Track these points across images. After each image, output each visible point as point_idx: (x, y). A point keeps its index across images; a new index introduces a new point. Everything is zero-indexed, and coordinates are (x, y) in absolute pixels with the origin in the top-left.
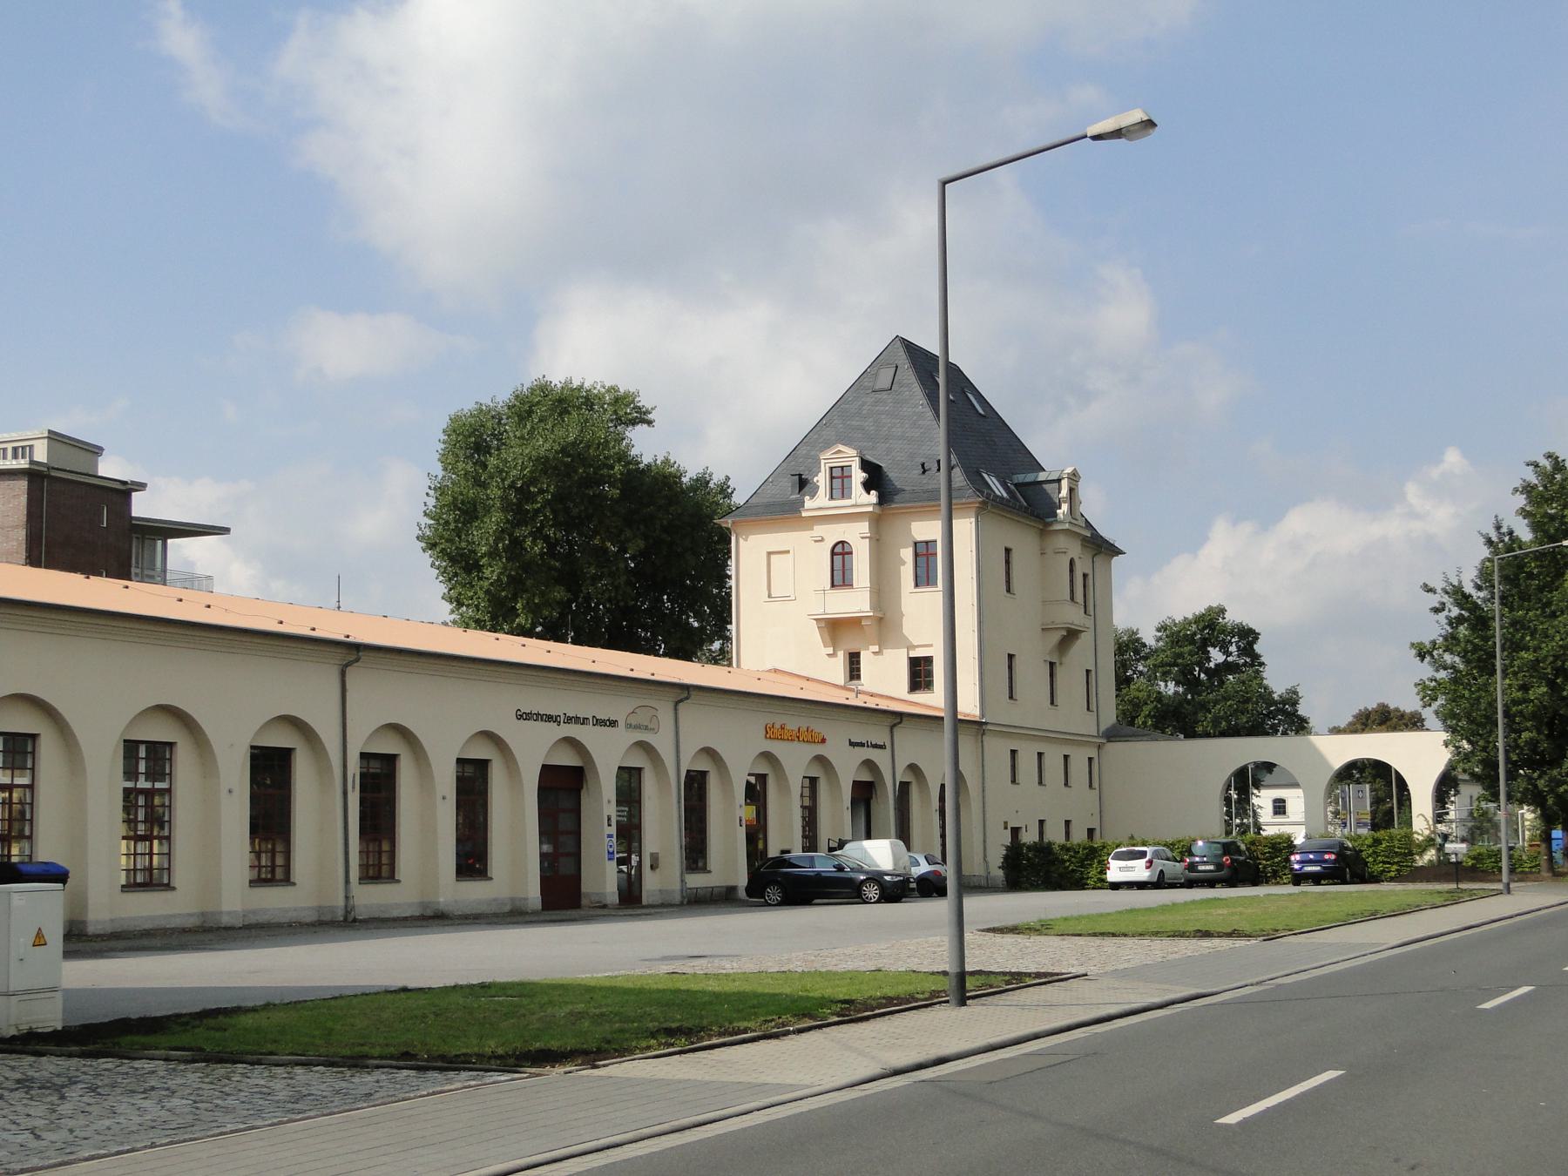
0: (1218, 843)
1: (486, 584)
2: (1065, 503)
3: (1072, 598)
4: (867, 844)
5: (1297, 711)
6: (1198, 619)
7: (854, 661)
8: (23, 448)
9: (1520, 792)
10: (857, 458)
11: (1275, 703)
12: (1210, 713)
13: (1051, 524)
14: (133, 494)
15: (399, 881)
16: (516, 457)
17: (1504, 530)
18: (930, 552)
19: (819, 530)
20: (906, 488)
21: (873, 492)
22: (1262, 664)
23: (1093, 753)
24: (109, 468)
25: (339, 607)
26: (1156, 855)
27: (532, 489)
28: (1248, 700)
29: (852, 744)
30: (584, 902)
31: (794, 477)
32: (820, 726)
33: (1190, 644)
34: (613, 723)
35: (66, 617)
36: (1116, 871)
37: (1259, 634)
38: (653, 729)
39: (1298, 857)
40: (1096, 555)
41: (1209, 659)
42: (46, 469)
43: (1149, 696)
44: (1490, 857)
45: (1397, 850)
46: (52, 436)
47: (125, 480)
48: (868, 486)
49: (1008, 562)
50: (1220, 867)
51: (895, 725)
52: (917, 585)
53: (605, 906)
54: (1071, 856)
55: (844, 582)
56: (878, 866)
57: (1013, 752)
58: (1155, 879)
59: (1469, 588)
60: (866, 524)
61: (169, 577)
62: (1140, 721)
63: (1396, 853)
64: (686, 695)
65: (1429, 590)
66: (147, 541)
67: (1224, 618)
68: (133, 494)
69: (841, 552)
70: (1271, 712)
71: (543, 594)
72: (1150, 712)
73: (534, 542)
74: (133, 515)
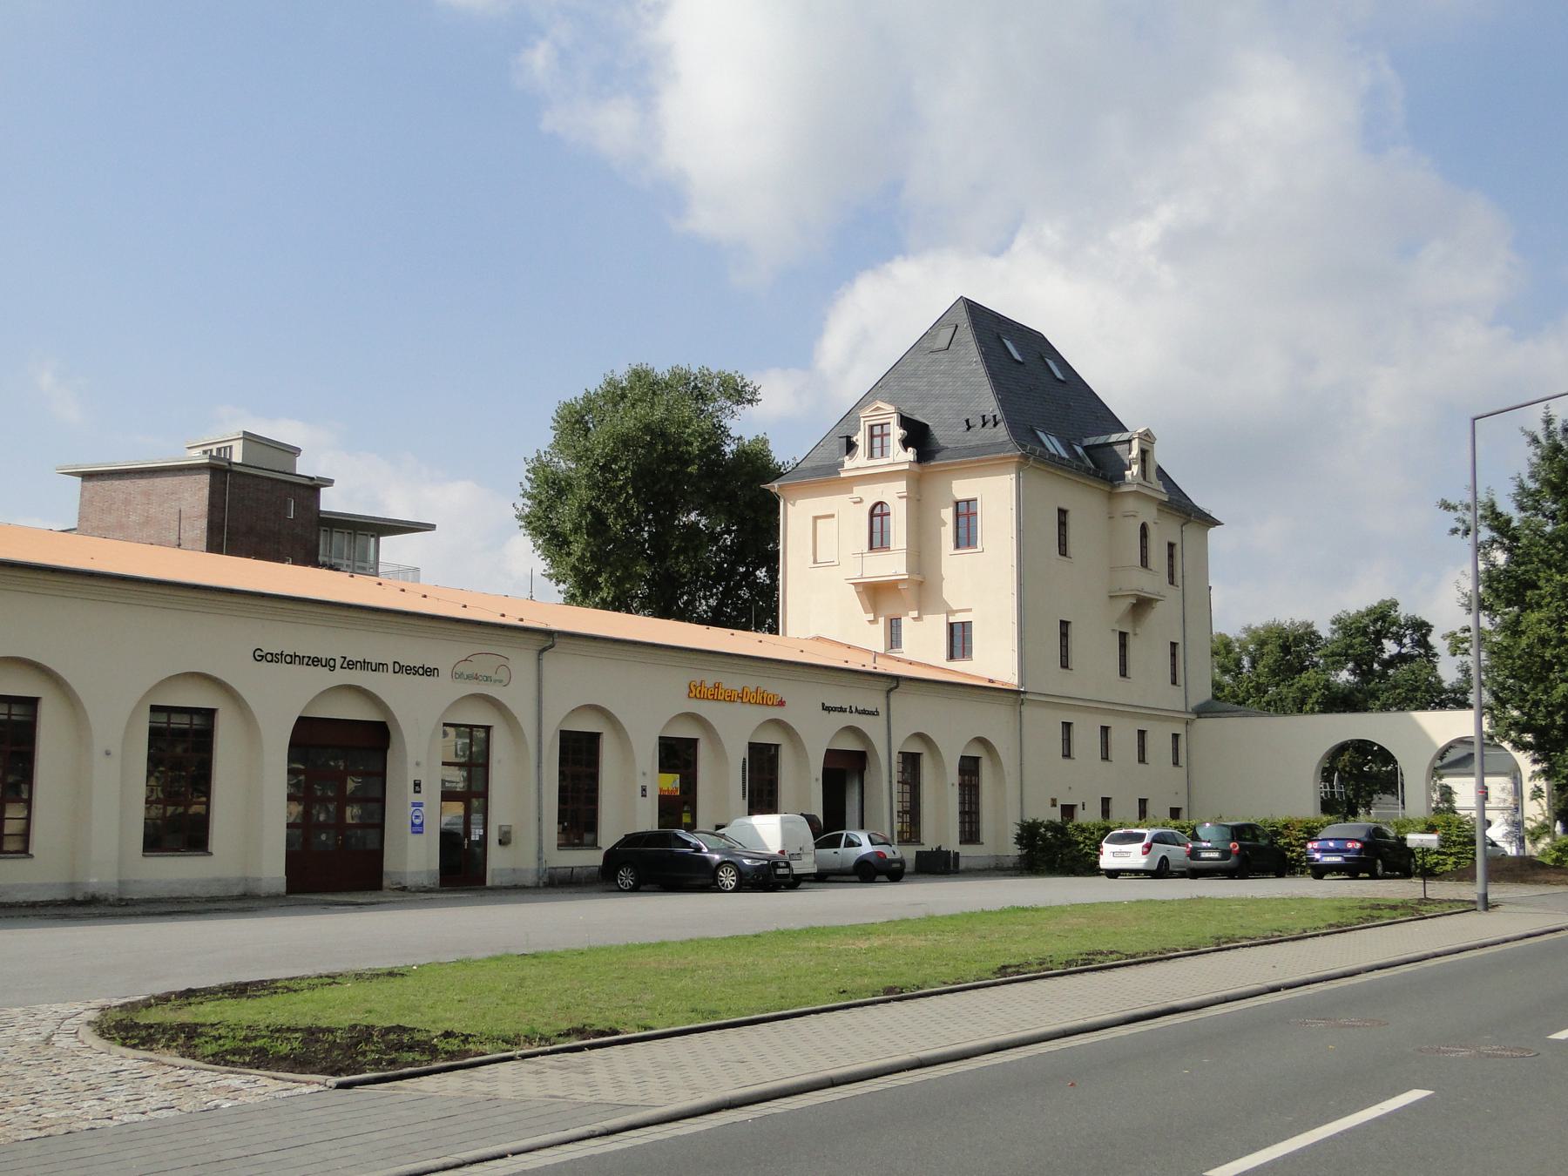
1: (573, 559)
3: (1144, 562)
4: (757, 820)
5: (1468, 700)
6: (1370, 612)
8: (225, 448)
10: (895, 415)
11: (1445, 691)
12: (1379, 700)
14: (322, 489)
15: (32, 856)
16: (600, 439)
18: (971, 511)
19: (859, 491)
20: (949, 446)
21: (910, 449)
22: (1435, 655)
23: (1179, 729)
24: (305, 467)
25: (531, 597)
26: (1158, 839)
27: (613, 466)
28: (1417, 689)
29: (826, 708)
30: (386, 883)
31: (841, 439)
32: (775, 686)
33: (1362, 635)
34: (429, 672)
35: (335, 612)
36: (1110, 856)
37: (1432, 626)
38: (501, 681)
39: (1316, 845)
40: (1184, 524)
41: (1382, 650)
42: (226, 464)
43: (1318, 684)
45: (1454, 838)
47: (312, 476)
48: (906, 443)
50: (1226, 854)
51: (891, 690)
52: (957, 546)
53: (404, 889)
54: (1086, 838)
55: (882, 544)
56: (769, 850)
58: (1154, 867)
59: (1507, 507)
60: (904, 483)
63: (1454, 842)
65: (1447, 506)
66: (358, 536)
68: (322, 489)
69: (878, 513)
70: (1442, 700)
71: (626, 568)
74: (321, 509)
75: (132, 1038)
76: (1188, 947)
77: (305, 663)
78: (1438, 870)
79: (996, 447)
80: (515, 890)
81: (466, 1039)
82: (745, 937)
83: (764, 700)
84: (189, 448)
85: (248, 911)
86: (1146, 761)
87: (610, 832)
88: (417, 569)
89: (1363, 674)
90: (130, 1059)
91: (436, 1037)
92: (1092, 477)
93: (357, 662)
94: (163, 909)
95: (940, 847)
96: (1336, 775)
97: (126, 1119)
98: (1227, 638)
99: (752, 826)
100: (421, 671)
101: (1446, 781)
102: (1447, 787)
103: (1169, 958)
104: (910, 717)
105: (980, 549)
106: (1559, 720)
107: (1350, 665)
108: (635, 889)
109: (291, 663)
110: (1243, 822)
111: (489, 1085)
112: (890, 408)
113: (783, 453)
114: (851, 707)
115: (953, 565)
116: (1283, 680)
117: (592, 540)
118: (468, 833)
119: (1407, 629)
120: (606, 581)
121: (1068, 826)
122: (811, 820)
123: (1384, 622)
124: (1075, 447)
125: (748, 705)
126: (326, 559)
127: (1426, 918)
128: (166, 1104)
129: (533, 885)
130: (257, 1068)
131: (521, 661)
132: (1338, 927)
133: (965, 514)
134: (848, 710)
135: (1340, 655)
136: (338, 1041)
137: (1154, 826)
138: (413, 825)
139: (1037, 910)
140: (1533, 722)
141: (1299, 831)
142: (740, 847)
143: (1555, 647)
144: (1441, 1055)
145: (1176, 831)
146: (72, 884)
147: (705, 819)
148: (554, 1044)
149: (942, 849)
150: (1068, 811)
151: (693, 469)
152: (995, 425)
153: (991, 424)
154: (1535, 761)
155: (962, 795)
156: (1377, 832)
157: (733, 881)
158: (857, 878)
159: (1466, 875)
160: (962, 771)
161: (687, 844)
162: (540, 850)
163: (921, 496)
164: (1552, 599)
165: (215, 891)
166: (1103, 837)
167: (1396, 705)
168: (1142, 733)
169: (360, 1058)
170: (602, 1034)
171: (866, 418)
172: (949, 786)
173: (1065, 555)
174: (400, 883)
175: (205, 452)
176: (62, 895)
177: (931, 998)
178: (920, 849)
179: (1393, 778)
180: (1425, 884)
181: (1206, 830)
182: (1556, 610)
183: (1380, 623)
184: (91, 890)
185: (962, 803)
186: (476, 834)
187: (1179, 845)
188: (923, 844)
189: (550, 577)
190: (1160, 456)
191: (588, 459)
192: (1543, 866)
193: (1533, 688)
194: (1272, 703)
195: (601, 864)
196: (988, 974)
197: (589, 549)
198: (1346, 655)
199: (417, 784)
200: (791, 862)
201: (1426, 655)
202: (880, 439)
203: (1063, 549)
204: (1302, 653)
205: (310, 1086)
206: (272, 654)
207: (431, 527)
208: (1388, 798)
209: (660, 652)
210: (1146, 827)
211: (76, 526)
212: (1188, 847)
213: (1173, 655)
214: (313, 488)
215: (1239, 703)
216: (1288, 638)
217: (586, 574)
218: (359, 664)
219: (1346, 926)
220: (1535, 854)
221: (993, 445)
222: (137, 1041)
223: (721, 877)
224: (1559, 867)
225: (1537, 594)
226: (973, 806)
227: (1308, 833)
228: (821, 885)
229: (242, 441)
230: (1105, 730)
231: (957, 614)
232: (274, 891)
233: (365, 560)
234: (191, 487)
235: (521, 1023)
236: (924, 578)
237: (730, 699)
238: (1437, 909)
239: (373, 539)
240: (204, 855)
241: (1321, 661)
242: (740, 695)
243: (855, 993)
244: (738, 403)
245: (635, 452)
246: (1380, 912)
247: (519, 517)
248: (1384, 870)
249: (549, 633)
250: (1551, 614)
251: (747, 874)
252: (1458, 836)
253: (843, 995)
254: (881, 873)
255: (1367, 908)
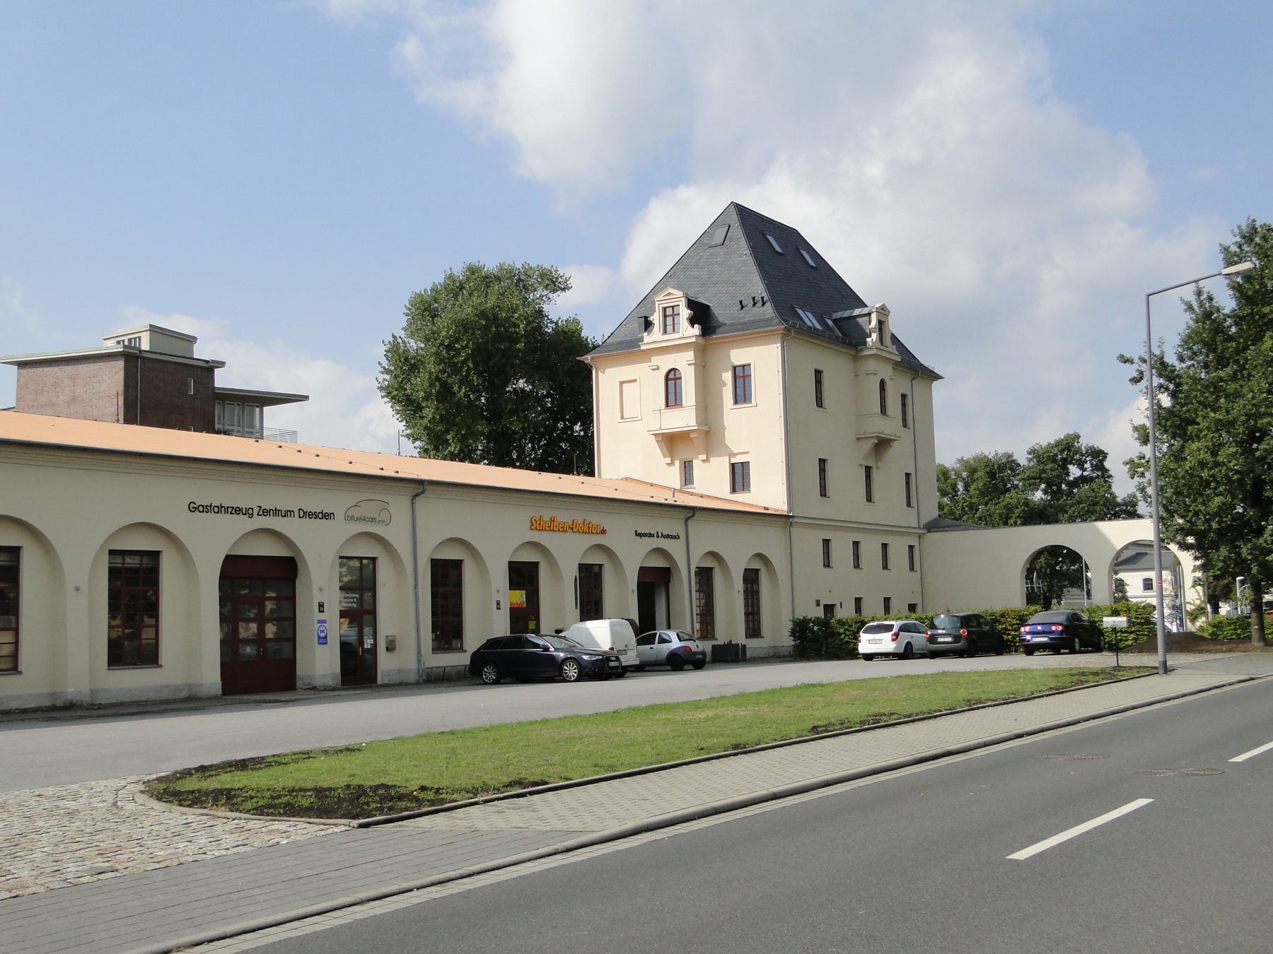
0: (956, 616)
1: (426, 421)
2: (874, 332)
4: (592, 625)
5: (1136, 511)
6: (1058, 443)
7: (687, 468)
8: (135, 339)
9: (1221, 561)
10: (684, 298)
11: (1119, 505)
12: (1067, 513)
13: (862, 350)
14: (216, 370)
15: (763, 637)
16: (444, 324)
17: (1204, 296)
19: (656, 360)
21: (696, 326)
22: (1110, 476)
24: (202, 352)
25: (399, 453)
27: (456, 345)
28: (1096, 503)
29: (638, 535)
30: (299, 684)
32: (598, 518)
33: (1053, 462)
34: (327, 516)
36: (867, 643)
37: (1107, 454)
38: (383, 521)
39: (1027, 629)
41: (1068, 474)
42: (138, 352)
43: (1019, 502)
44: (1230, 624)
46: (154, 329)
47: (208, 359)
48: (692, 321)
49: (904, 405)
50: (957, 639)
52: (736, 402)
53: (314, 688)
54: (846, 630)
56: (600, 647)
57: (856, 544)
59: (1171, 359)
60: (692, 353)
61: (265, 433)
62: (1012, 521)
64: (421, 490)
67: (1079, 442)
68: (216, 370)
69: (672, 377)
70: (1116, 512)
71: (469, 428)
72: (1019, 514)
73: (460, 388)
74: (216, 385)
75: (185, 800)
76: (948, 708)
77: (229, 512)
78: (1122, 645)
79: (766, 322)
80: (400, 686)
81: (438, 790)
82: (607, 714)
83: (589, 530)
84: (105, 339)
85: (198, 709)
86: (889, 568)
87: (474, 638)
88: (294, 432)
89: (1053, 493)
90: (177, 816)
91: (415, 791)
92: (840, 344)
93: (270, 510)
94: (129, 710)
95: (731, 641)
96: (1035, 573)
97: (217, 853)
98: (945, 467)
99: (587, 629)
100: (320, 516)
101: (1121, 575)
102: (1121, 580)
103: (935, 717)
104: (705, 539)
105: (754, 403)
106: (1215, 526)
107: (1043, 486)
108: (497, 682)
109: (218, 512)
110: (969, 613)
111: (468, 822)
112: (679, 293)
113: (593, 332)
114: (657, 533)
115: (733, 418)
116: (991, 500)
117: (440, 405)
118: (361, 643)
119: (1088, 457)
120: (454, 438)
121: (832, 621)
122: (631, 622)
123: (1069, 451)
124: (827, 320)
125: (577, 534)
126: (221, 426)
127: (1121, 681)
128: (241, 843)
129: (415, 682)
130: (294, 816)
131: (399, 505)
132: (1057, 689)
133: (742, 376)
134: (655, 535)
135: (1035, 478)
136: (342, 796)
137: (899, 619)
138: (319, 638)
139: (823, 686)
140: (1195, 527)
141: (1013, 618)
142: (579, 646)
143: (1211, 469)
144: (1154, 775)
145: (917, 622)
146: (54, 694)
147: (545, 626)
148: (504, 792)
149: (733, 643)
150: (829, 609)
151: (520, 346)
152: (763, 304)
153: (760, 304)
154: (1196, 558)
155: (746, 599)
156: (1074, 618)
157: (575, 673)
158: (669, 668)
159: (1150, 647)
160: (746, 581)
161: (537, 646)
162: (419, 653)
163: (706, 363)
164: (1208, 431)
165: (165, 695)
166: (859, 629)
167: (1080, 517)
168: (885, 546)
169: (366, 807)
170: (536, 784)
171: (660, 302)
172: (630, 593)
173: (821, 407)
174: (310, 684)
175: (118, 342)
176: (46, 703)
177: (767, 751)
178: (715, 643)
179: (1079, 575)
180: (1117, 655)
181: (941, 620)
182: (1212, 440)
183: (1066, 452)
184: (69, 698)
185: (746, 605)
186: (368, 643)
187: (920, 633)
188: (717, 639)
189: (408, 436)
190: (893, 326)
191: (435, 340)
192: (1203, 639)
193: (1195, 500)
194: (983, 518)
195: (469, 663)
196: (805, 733)
197: (439, 412)
198: (1040, 478)
199: (321, 606)
200: (620, 656)
201: (1103, 476)
202: (671, 318)
203: (819, 402)
204: (1005, 478)
205: (338, 827)
206: (203, 506)
207: (305, 398)
208: (1075, 591)
209: (334, 478)
210: (893, 620)
211: (15, 405)
212: (927, 634)
213: (908, 483)
214: (208, 369)
215: (956, 519)
216: (994, 466)
217: (436, 434)
218: (271, 511)
219: (1063, 689)
220: (1195, 631)
221: (760, 321)
222: (190, 802)
223: (565, 670)
224: (1215, 639)
225: (1196, 429)
226: (755, 608)
227: (1020, 620)
228: (639, 674)
229: (149, 332)
230: (856, 544)
231: (737, 456)
232: (213, 694)
233: (252, 426)
234: (109, 371)
235: (472, 779)
236: (710, 428)
237: (563, 529)
238: (1128, 674)
239: (258, 409)
240: (15, 674)
241: (1021, 484)
242: (571, 526)
243: (710, 750)
244: (554, 291)
245: (473, 333)
246: (1086, 677)
247: (381, 389)
248: (1081, 646)
249: (420, 482)
250: (1207, 444)
251: (586, 667)
252: (1136, 618)
253: (702, 751)
254: (688, 663)
255: (1076, 675)
